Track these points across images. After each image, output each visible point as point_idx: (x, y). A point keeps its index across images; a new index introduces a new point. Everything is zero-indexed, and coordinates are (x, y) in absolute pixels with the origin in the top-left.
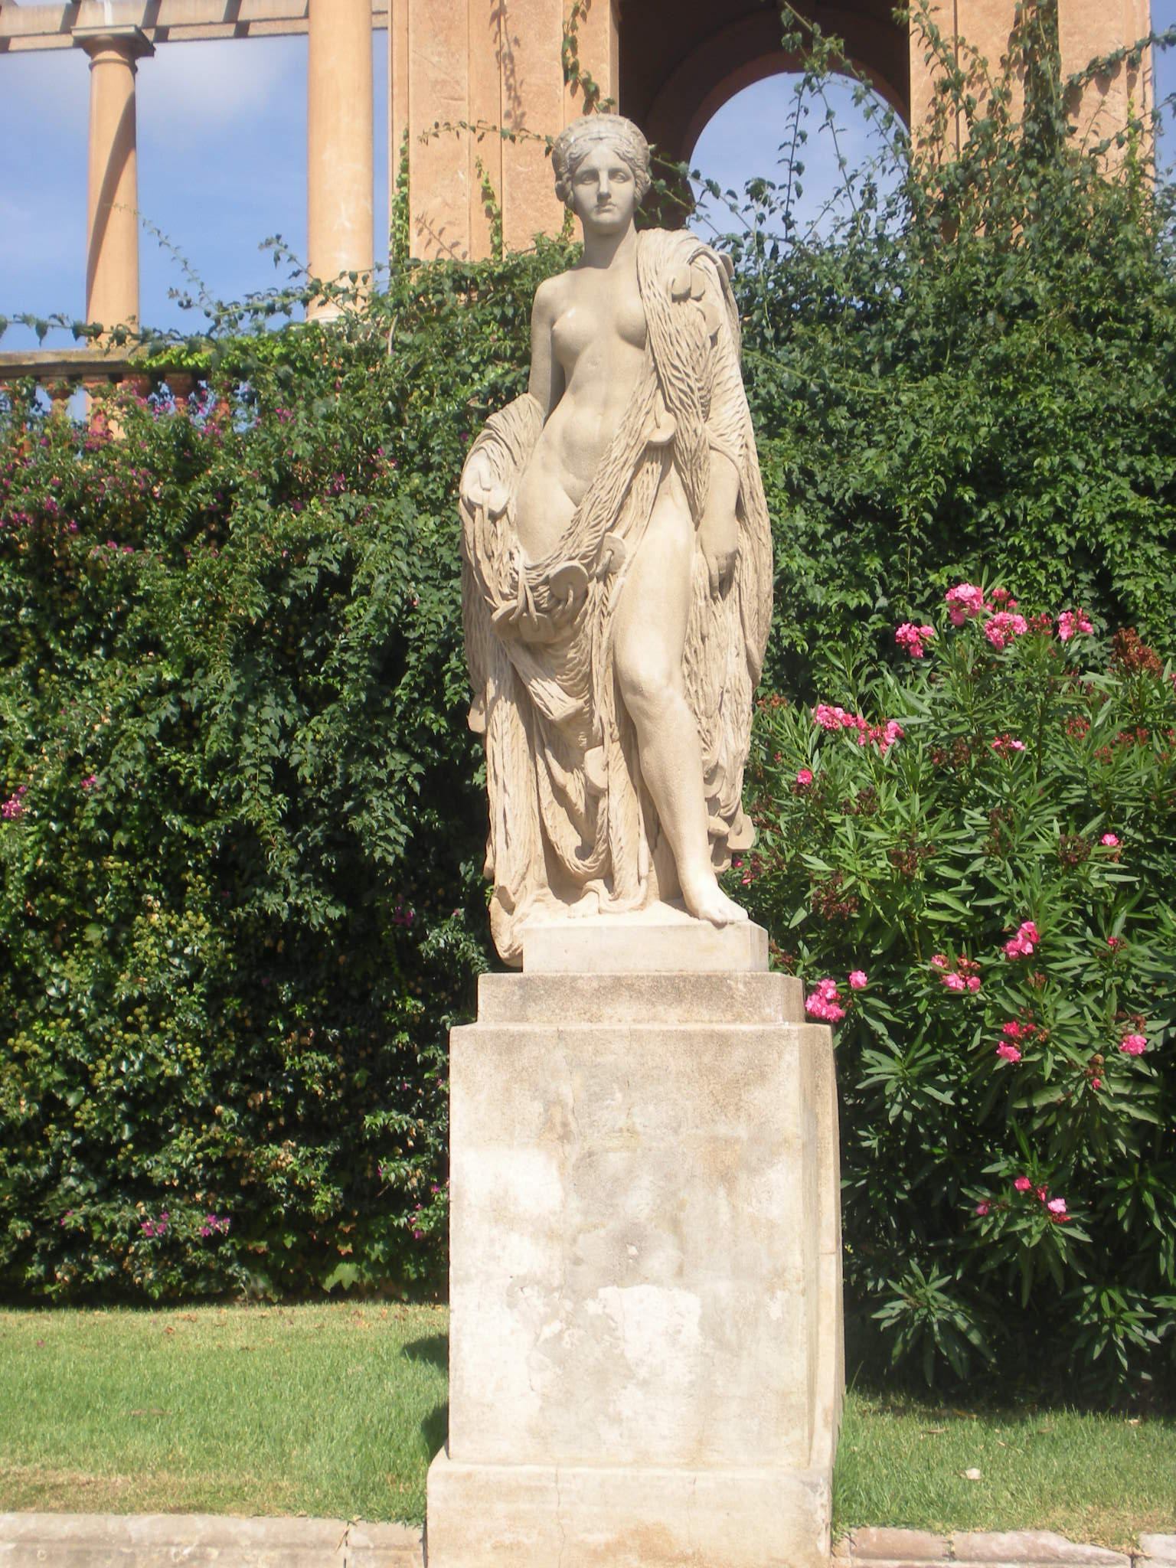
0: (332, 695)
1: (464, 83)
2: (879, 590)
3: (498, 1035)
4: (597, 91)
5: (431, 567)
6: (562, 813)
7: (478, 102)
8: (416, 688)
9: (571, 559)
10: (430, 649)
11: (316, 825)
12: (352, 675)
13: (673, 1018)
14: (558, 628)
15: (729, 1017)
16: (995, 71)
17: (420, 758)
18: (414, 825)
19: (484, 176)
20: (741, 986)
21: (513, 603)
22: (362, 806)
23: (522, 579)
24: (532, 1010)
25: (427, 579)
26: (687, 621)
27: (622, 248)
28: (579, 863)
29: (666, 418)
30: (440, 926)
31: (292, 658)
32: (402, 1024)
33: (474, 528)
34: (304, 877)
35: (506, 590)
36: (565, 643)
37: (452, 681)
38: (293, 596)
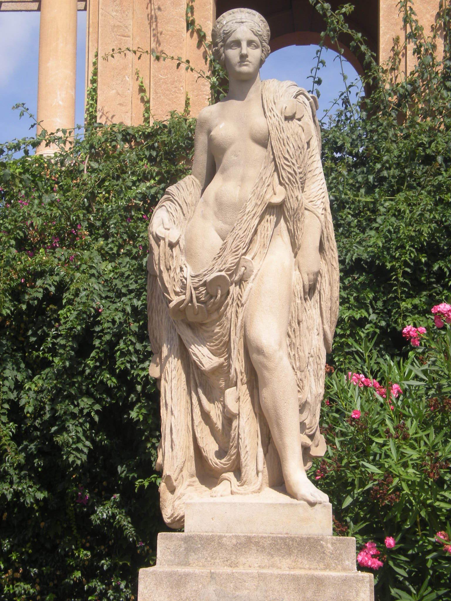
0: (48, 364)
1: (130, 28)
2: (371, 311)
3: (170, 575)
4: (204, 36)
5: (109, 291)
6: (207, 429)
7: (138, 39)
8: (99, 360)
9: (220, 271)
10: (107, 337)
11: (31, 441)
12: (62, 351)
13: (285, 566)
14: (209, 313)
15: (322, 566)
16: (427, 33)
17: (98, 401)
18: (93, 441)
19: (140, 79)
20: (329, 545)
21: (183, 297)
22: (63, 429)
23: (189, 283)
24: (193, 557)
25: (107, 297)
26: (290, 312)
27: (253, 89)
28: (218, 461)
29: (279, 189)
30: (104, 505)
31: (22, 342)
32: (77, 566)
33: (159, 251)
34: (23, 473)
35: (178, 290)
36: (213, 323)
37: (120, 357)
38: (28, 305)
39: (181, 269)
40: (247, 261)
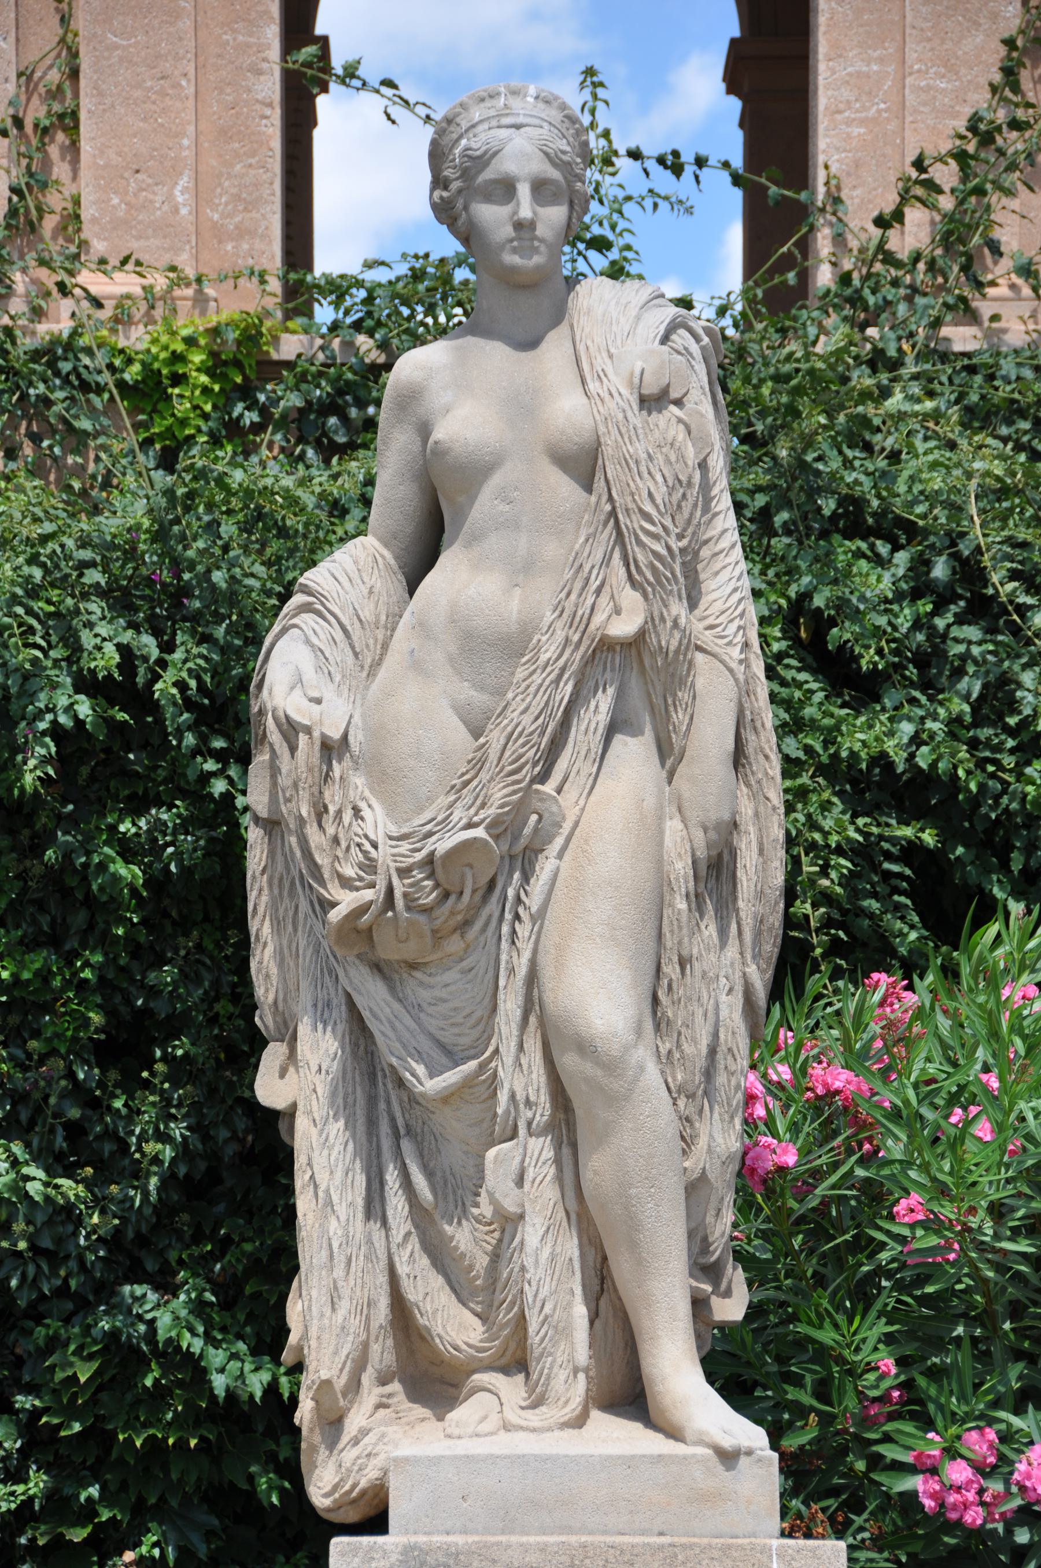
9: (470, 826)
21: (368, 895)
23: (384, 855)
29: (630, 597)
39: (357, 811)
40: (543, 797)
